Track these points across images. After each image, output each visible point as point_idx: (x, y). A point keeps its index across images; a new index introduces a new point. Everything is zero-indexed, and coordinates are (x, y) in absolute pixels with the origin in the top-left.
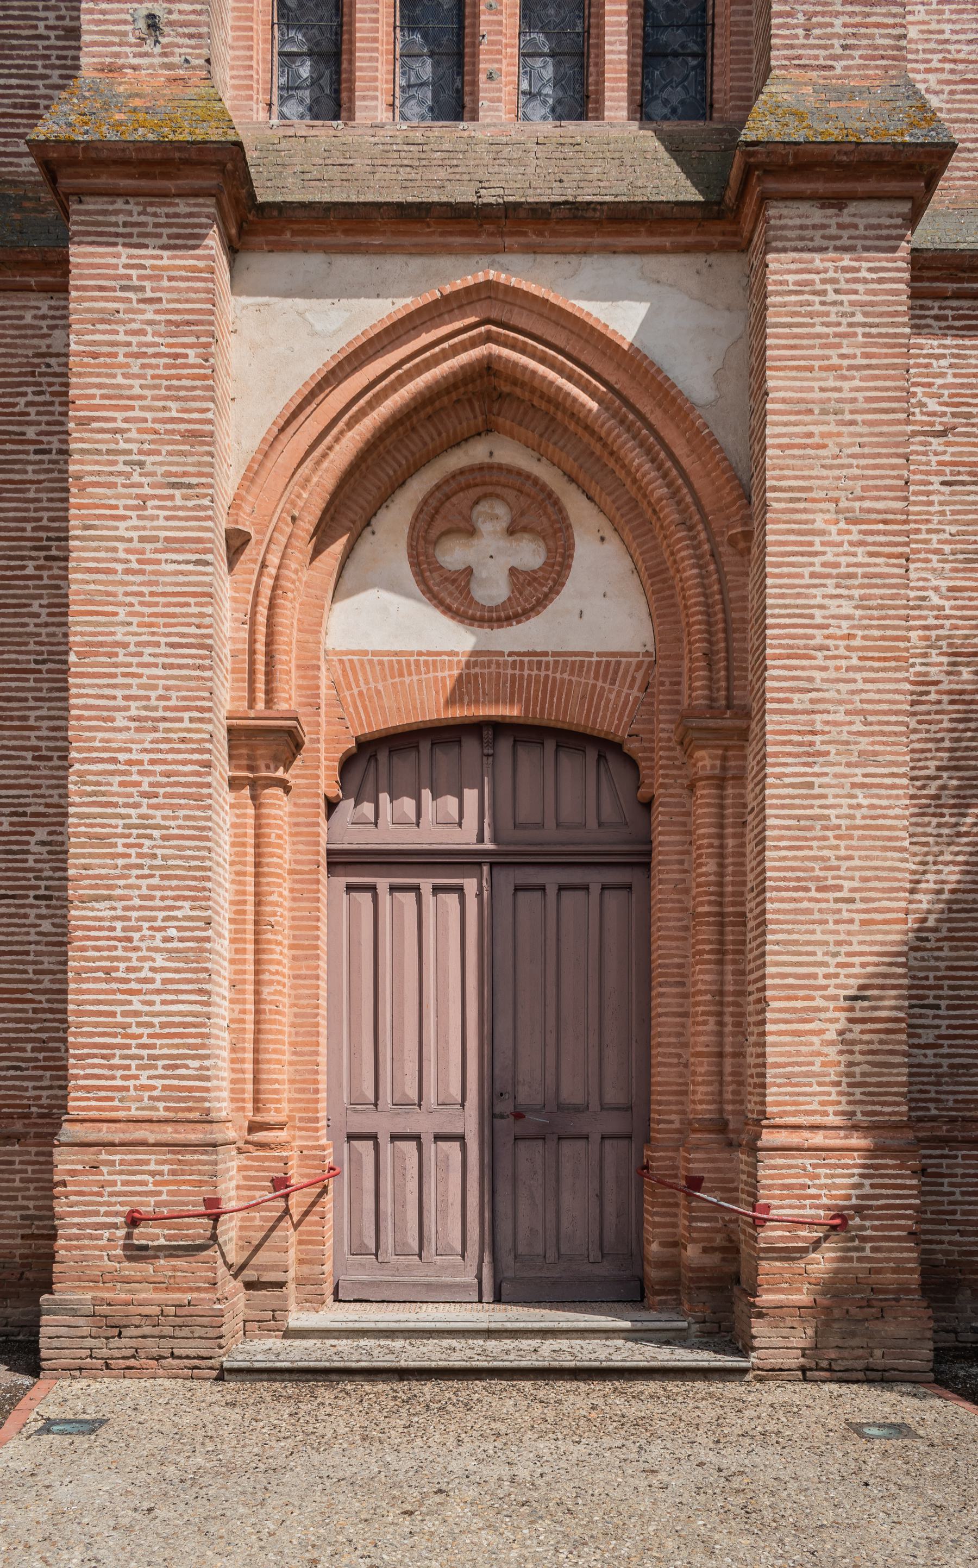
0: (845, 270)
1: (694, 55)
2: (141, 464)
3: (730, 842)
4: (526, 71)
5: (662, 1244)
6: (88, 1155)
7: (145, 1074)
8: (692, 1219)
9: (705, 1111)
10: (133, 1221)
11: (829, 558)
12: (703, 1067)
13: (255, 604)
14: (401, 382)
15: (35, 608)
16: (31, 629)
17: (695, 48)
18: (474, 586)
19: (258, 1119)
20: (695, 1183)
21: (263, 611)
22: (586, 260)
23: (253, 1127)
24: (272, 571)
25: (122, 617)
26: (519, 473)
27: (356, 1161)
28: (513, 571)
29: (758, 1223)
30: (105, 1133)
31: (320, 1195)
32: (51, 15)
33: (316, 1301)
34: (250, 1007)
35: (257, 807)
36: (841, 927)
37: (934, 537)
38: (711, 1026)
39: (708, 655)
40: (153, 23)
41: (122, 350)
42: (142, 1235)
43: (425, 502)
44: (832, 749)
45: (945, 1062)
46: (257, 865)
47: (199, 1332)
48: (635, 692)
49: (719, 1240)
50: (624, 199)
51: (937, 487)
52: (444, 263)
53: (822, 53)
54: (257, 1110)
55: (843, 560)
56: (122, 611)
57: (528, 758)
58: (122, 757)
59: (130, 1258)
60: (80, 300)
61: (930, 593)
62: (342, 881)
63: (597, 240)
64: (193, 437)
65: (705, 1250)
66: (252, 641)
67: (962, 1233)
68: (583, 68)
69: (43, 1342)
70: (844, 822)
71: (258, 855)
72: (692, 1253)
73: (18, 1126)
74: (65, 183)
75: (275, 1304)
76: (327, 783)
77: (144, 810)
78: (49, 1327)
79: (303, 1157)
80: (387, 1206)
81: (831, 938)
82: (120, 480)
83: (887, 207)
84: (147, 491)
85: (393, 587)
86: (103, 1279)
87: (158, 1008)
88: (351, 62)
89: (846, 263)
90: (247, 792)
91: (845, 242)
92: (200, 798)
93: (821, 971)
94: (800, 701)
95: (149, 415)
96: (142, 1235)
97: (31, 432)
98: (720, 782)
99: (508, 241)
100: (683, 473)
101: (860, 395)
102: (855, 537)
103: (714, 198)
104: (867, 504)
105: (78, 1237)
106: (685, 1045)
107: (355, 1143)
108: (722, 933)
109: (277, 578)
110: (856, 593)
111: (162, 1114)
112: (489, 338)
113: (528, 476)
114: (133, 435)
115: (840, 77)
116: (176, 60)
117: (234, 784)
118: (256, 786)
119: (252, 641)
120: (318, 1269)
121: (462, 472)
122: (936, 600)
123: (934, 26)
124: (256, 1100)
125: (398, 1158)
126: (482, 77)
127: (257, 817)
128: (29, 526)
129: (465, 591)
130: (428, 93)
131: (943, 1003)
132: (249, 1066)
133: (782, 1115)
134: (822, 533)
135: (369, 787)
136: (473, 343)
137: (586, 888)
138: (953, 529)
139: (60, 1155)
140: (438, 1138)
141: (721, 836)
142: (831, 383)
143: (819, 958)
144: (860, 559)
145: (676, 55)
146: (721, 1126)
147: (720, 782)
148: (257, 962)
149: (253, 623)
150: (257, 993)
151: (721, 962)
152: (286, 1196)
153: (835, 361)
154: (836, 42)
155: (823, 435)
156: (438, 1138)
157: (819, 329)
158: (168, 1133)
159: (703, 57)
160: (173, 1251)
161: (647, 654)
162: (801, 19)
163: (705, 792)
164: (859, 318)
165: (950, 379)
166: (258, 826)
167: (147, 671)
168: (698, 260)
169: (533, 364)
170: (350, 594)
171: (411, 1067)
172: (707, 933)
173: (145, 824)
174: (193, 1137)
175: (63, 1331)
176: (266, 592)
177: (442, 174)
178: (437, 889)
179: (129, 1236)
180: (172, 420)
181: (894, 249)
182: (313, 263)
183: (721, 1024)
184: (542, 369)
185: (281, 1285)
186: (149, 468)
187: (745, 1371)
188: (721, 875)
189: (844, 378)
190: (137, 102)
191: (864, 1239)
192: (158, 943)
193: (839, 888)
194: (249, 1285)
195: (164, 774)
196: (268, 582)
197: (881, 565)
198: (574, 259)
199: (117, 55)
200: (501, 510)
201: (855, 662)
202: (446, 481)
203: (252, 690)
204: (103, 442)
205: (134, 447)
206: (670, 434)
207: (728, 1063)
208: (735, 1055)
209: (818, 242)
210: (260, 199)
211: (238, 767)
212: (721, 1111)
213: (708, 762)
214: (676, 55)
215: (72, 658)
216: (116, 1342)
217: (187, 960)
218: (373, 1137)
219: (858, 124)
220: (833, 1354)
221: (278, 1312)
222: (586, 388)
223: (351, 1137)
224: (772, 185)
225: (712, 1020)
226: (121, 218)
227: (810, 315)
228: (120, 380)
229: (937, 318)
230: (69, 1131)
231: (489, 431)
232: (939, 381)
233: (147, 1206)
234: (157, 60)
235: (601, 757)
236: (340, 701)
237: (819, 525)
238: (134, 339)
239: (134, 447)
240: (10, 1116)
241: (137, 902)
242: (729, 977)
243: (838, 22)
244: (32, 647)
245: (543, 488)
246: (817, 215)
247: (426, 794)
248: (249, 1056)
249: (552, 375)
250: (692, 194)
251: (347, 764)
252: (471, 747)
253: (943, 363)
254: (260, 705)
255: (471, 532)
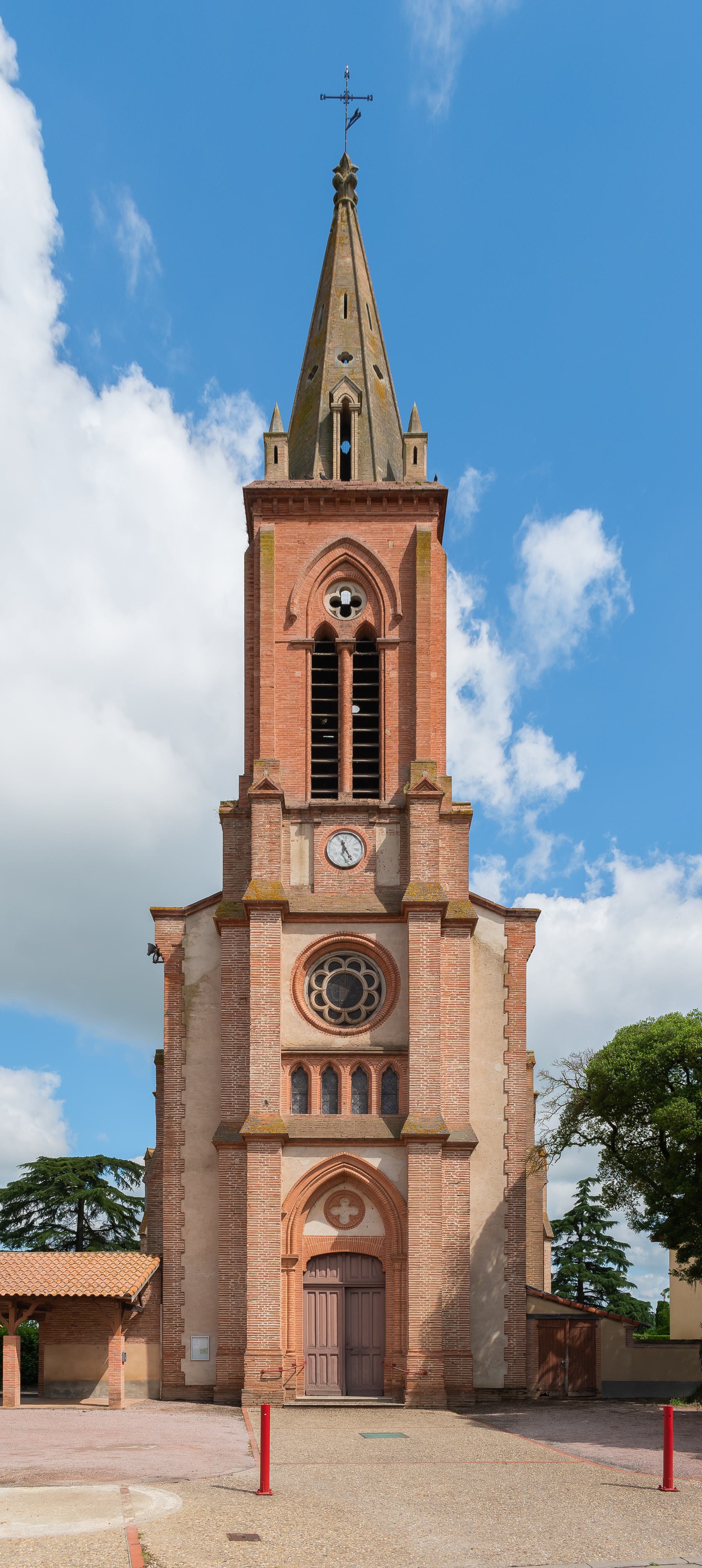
0: (426, 1158)
1: (395, 1094)
2: (264, 1202)
3: (403, 1285)
4: (353, 1097)
5: (387, 1380)
6: (252, 1358)
7: (265, 1339)
8: (393, 1374)
9: (397, 1348)
10: (263, 1372)
11: (423, 1223)
12: (397, 1338)
13: (288, 1229)
14: (323, 1176)
15: (231, 1226)
16: (230, 1231)
17: (395, 1093)
18: (340, 1219)
19: (289, 1350)
20: (394, 1365)
21: (289, 1230)
22: (367, 1148)
23: (287, 1352)
24: (292, 1220)
25: (259, 1236)
26: (352, 1192)
27: (310, 1360)
28: (350, 1216)
29: (407, 1373)
30: (256, 1353)
31: (303, 1368)
32: (235, 1082)
33: (301, 1394)
34: (286, 1323)
35: (288, 1276)
36: (426, 1307)
37: (455, 1209)
38: (398, 1328)
39: (397, 1241)
40: (266, 1102)
41: (259, 1176)
42: (264, 1376)
43: (328, 1199)
44: (424, 1266)
45: (459, 1336)
46: (288, 1290)
47: (278, 1397)
48: (381, 1246)
49: (400, 1379)
50: (376, 1137)
51: (456, 1196)
52: (333, 1149)
53: (421, 1109)
54: (288, 1348)
55: (426, 1223)
56: (259, 1235)
57: (354, 1261)
58: (259, 1268)
59: (261, 1381)
60: (249, 1165)
61: (454, 1222)
62: (307, 1291)
63: (370, 1144)
64: (276, 1196)
65: (397, 1381)
66: (287, 1237)
67: (463, 1378)
68: (367, 1097)
69: (242, 1399)
70: (427, 1283)
71: (288, 1287)
72: (394, 1381)
73: (227, 1352)
74: (246, 1140)
75: (293, 1393)
76: (304, 1268)
77: (264, 1280)
78: (244, 1397)
79: (298, 1359)
80: (318, 1372)
81: (424, 1309)
82: (259, 1205)
83: (436, 1144)
84: (265, 1208)
85: (320, 1220)
86: (256, 1386)
87: (268, 1324)
88: (311, 1097)
89: (427, 1157)
90: (286, 1273)
91: (426, 1152)
92: (278, 1277)
93: (421, 1316)
94: (416, 1255)
95: (266, 1191)
96: (264, 1376)
97: (230, 1183)
98: (400, 1270)
99: (349, 1144)
100: (391, 1198)
101: (430, 1186)
102: (429, 1218)
103: (397, 1137)
104: (432, 1211)
105: (250, 1376)
106: (393, 1332)
107: (321, 1356)
108: (401, 1306)
109: (293, 1222)
110: (429, 1231)
111: (269, 1348)
112: (344, 1166)
113: (354, 1193)
114: (262, 1195)
115: (425, 1115)
116: (271, 1110)
117: (283, 1271)
118: (288, 1271)
119: (287, 1237)
120: (302, 1386)
121: (337, 1192)
122: (456, 1224)
123: (455, 1085)
124: (288, 1346)
125: (321, 1360)
126: (342, 1103)
127: (288, 1278)
128: (229, 1206)
129: (338, 1220)
130: (329, 1103)
131: (458, 1322)
132: (286, 1337)
133: (412, 1349)
134: (421, 1217)
135: (314, 1268)
136: (340, 1168)
137: (369, 1293)
138: (460, 1207)
139: (245, 1357)
140: (331, 1355)
141: (401, 1283)
142: (423, 1184)
143: (421, 1313)
144: (430, 1223)
145: (390, 1094)
146: (401, 1352)
147: (400, 1270)
148: (288, 1313)
149: (287, 1233)
150: (288, 1320)
151: (401, 1313)
152: (295, 1368)
153: (424, 1179)
154: (424, 1107)
155: (421, 1195)
156: (331, 1355)
157: (420, 1172)
158: (270, 1353)
159: (397, 1095)
160: (271, 1380)
161: (384, 1236)
162: (416, 1101)
163: (397, 1273)
164: (430, 1169)
165: (459, 1170)
166: (288, 1281)
167: (265, 1248)
168: (395, 1148)
169: (355, 1173)
170: (309, 1221)
171: (325, 1337)
172: (398, 1306)
173: (265, 1283)
174: (276, 1354)
175: (247, 1397)
176: (290, 1225)
177: (333, 1130)
178: (331, 1293)
179: (261, 1376)
180: (271, 1192)
181: (437, 1154)
182: (302, 1149)
183: (401, 1328)
184: (357, 1174)
185: (294, 1389)
186: (265, 1203)
187: (403, 1406)
188: (401, 1292)
189: (426, 1182)
190: (263, 1122)
191: (431, 1377)
192: (268, 1310)
193: (426, 1298)
194: (287, 1389)
195: (269, 1272)
196: (291, 1223)
197: (435, 1225)
198: (364, 1148)
199: (258, 1109)
200: (347, 1200)
201: (429, 1246)
202: (333, 1194)
203: (287, 1249)
204: (255, 1197)
205: (262, 1198)
206: (388, 1189)
207: (402, 1337)
208: (404, 1335)
209: (420, 1152)
210: (290, 1137)
211: (283, 1267)
212: (401, 1348)
213: (397, 1266)
214: (390, 1094)
215: (248, 1245)
216: (259, 1400)
217: (274, 1314)
218: (315, 1355)
219: (428, 1129)
220: (424, 1403)
221: (293, 1396)
222: (367, 1178)
223: (309, 1355)
224: (409, 1140)
225: (398, 1327)
226: (259, 1147)
227: (419, 1168)
228: (259, 1183)
229: (456, 1155)
230: (247, 1352)
231: (344, 1182)
232: (457, 1171)
233: (266, 1369)
234: (267, 1111)
235: (373, 1260)
236: (307, 1248)
237: (421, 1216)
238: (262, 1174)
239: (262, 1198)
240: (225, 1349)
241: (263, 1301)
242: (403, 1317)
243: (425, 1102)
244: (230, 1235)
245: (358, 1196)
246: (420, 1146)
247: (328, 1270)
248: (286, 1335)
249: (359, 1175)
250: (392, 1137)
251: (308, 1263)
252: (339, 1258)
253: (457, 1166)
254: (289, 1253)
255: (340, 1206)
